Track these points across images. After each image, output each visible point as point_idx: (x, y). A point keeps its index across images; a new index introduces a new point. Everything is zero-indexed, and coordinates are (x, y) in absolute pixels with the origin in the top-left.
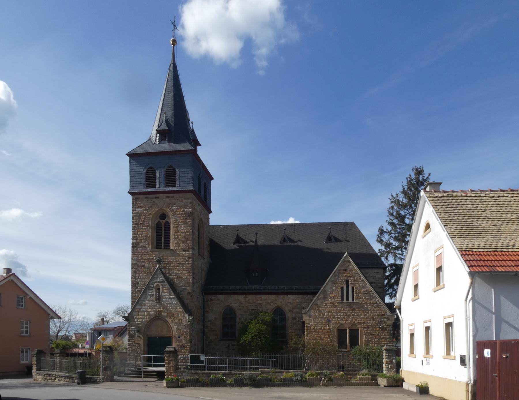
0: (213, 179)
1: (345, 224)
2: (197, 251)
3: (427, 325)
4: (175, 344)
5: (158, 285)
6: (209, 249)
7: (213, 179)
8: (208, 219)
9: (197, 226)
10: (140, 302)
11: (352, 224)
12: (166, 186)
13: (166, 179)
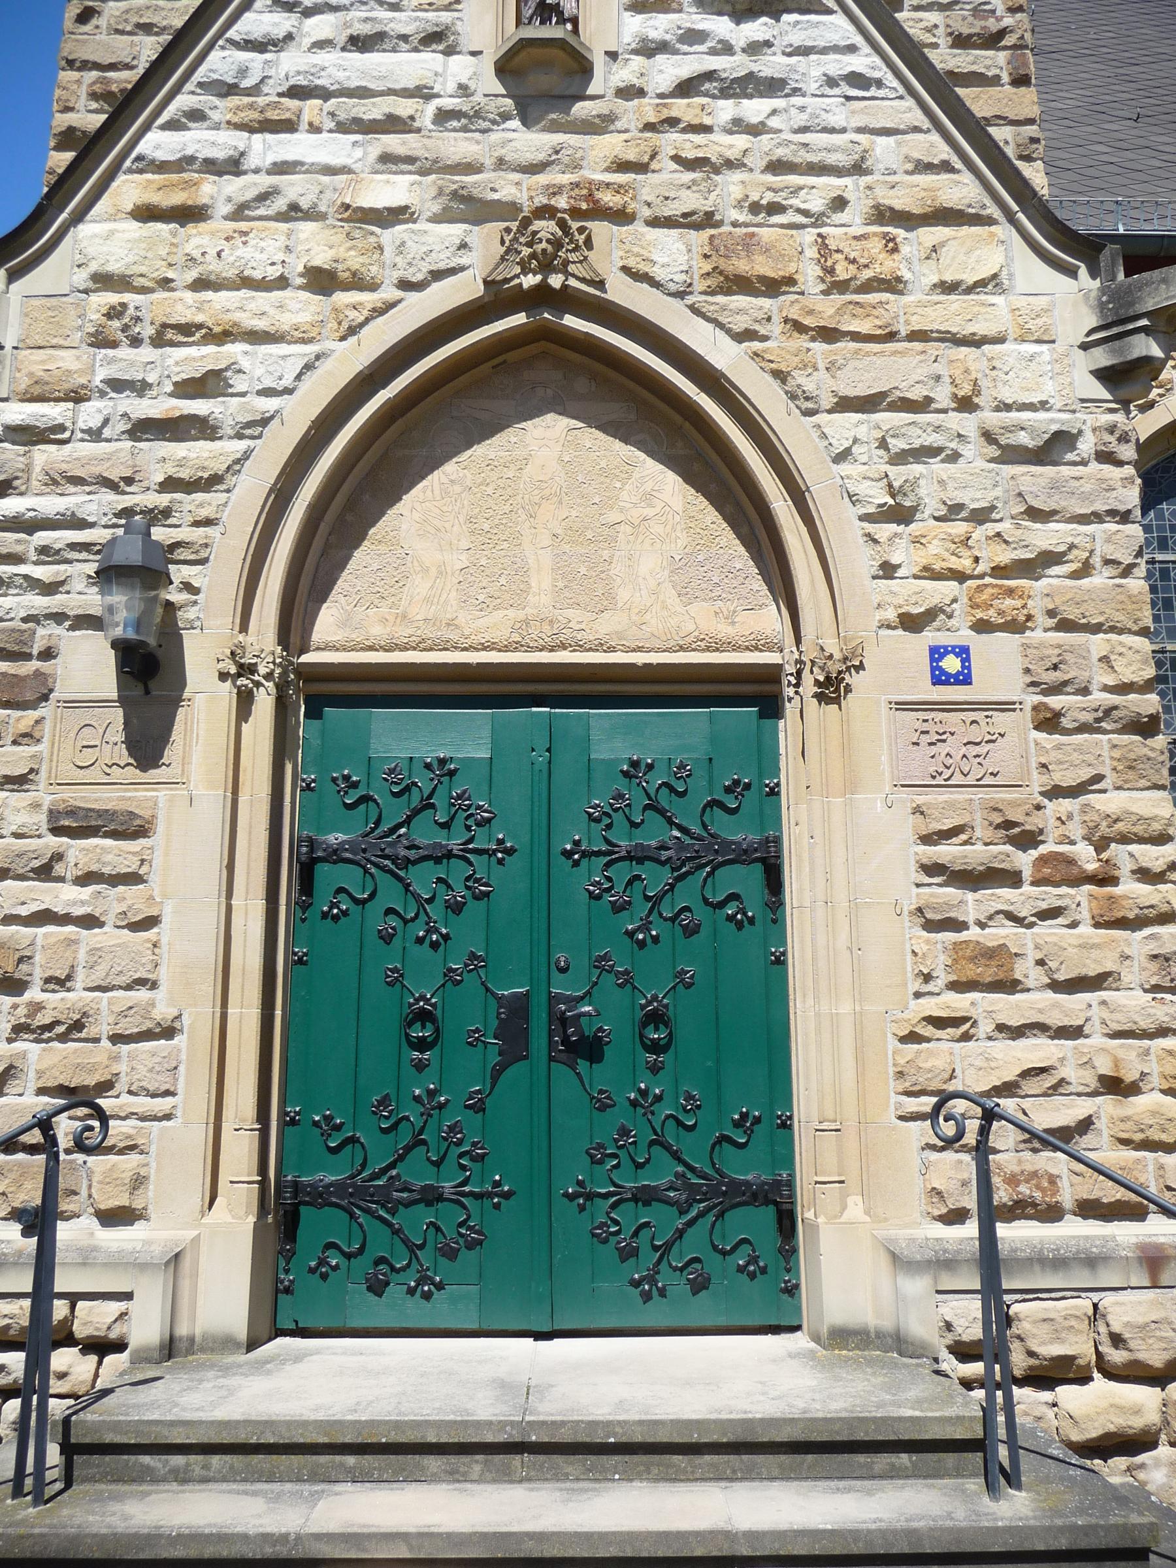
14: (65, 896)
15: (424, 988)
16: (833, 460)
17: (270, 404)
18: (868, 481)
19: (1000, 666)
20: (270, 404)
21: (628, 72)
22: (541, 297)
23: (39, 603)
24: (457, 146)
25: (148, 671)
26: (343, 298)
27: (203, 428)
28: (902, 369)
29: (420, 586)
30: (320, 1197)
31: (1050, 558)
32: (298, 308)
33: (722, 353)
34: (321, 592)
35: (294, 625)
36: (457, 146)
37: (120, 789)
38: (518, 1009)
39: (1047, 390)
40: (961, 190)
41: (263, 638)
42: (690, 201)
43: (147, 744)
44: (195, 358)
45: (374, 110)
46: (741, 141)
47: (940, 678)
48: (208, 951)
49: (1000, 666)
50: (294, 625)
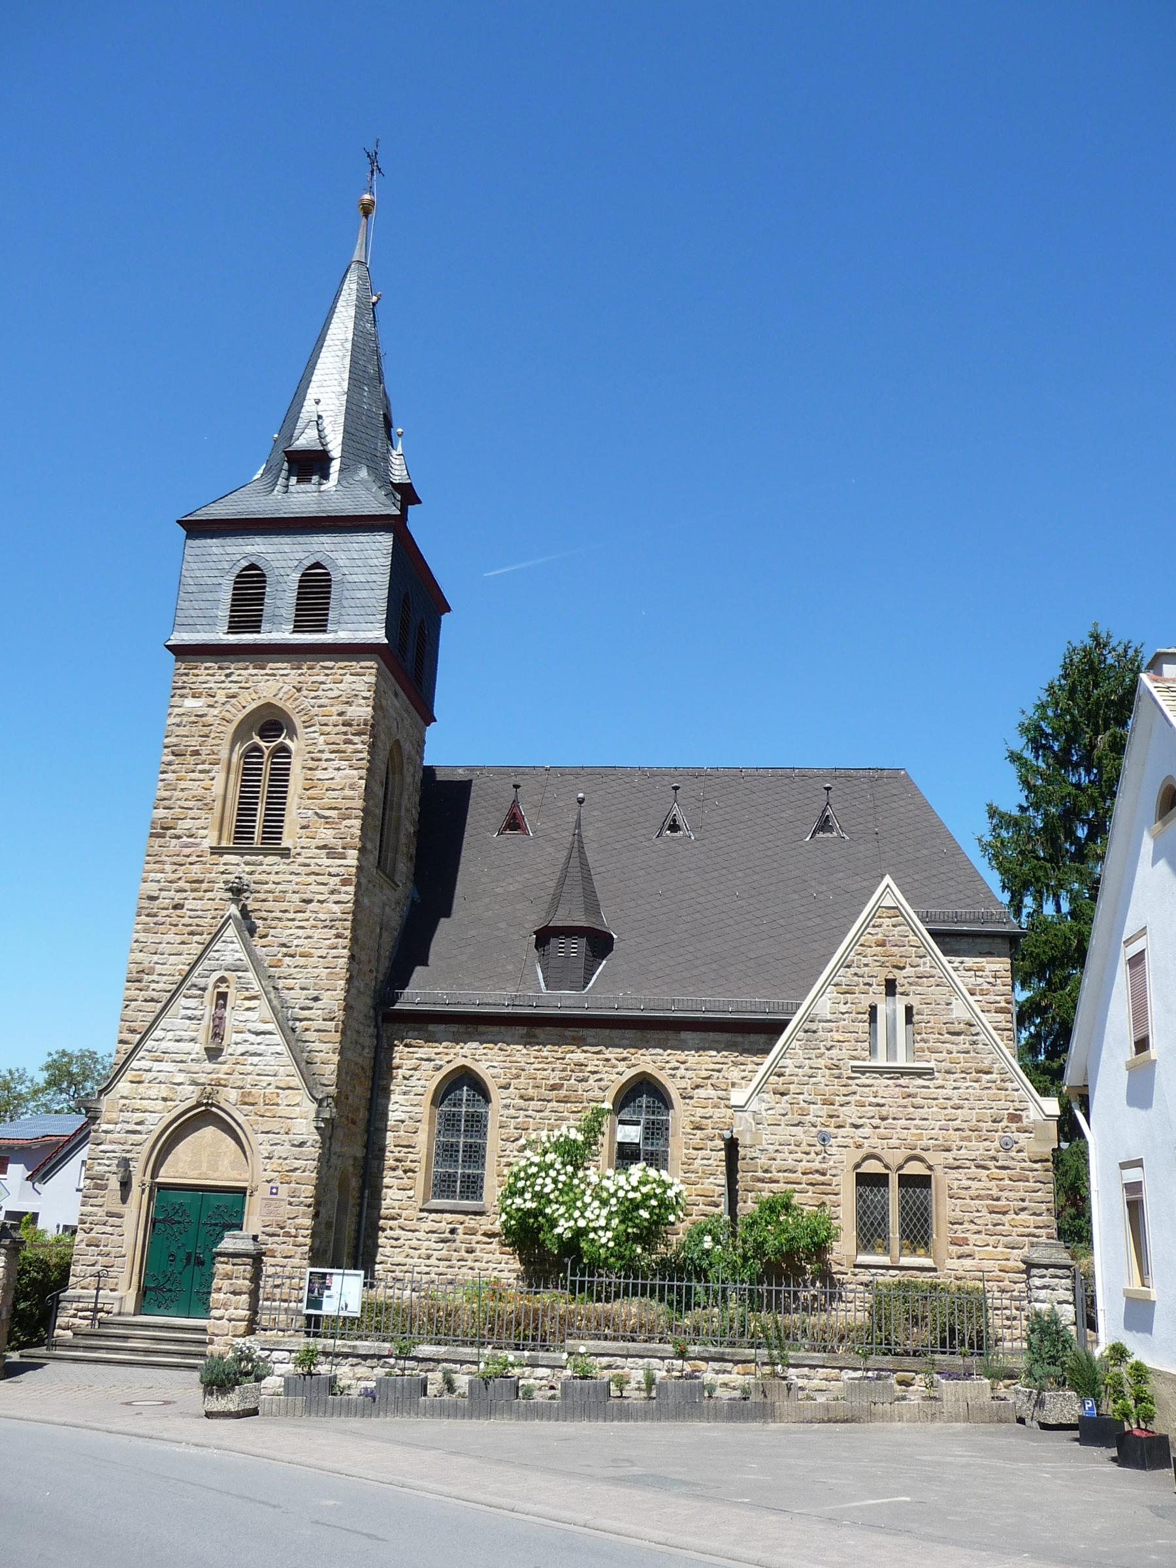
0: (449, 610)
1: (876, 776)
2: (373, 858)
3: (1132, 1175)
4: (254, 1222)
5: (223, 980)
6: (413, 851)
7: (449, 610)
8: (420, 744)
9: (383, 767)
10: (149, 1044)
11: (895, 775)
12: (298, 629)
13: (299, 607)
14: (108, 1229)
15: (173, 1249)
16: (260, 1144)
17: (152, 1127)
18: (265, 1150)
19: (284, 1190)
20: (152, 1127)
21: (230, 1051)
22: (207, 1104)
23: (107, 1169)
24: (195, 1067)
25: (125, 1185)
26: (169, 1103)
27: (139, 1132)
28: (274, 1125)
29: (181, 1164)
30: (151, 1289)
31: (297, 1169)
32: (160, 1105)
33: (241, 1119)
34: (161, 1166)
35: (154, 1174)
36: (195, 1067)
37: (118, 1208)
38: (189, 1254)
39: (304, 1130)
40: (297, 1081)
41: (148, 1178)
42: (239, 1083)
43: (124, 1199)
44: (138, 1116)
45: (178, 1057)
46: (252, 1068)
47: (272, 1193)
48: (133, 1242)
49: (284, 1190)
50: (154, 1174)
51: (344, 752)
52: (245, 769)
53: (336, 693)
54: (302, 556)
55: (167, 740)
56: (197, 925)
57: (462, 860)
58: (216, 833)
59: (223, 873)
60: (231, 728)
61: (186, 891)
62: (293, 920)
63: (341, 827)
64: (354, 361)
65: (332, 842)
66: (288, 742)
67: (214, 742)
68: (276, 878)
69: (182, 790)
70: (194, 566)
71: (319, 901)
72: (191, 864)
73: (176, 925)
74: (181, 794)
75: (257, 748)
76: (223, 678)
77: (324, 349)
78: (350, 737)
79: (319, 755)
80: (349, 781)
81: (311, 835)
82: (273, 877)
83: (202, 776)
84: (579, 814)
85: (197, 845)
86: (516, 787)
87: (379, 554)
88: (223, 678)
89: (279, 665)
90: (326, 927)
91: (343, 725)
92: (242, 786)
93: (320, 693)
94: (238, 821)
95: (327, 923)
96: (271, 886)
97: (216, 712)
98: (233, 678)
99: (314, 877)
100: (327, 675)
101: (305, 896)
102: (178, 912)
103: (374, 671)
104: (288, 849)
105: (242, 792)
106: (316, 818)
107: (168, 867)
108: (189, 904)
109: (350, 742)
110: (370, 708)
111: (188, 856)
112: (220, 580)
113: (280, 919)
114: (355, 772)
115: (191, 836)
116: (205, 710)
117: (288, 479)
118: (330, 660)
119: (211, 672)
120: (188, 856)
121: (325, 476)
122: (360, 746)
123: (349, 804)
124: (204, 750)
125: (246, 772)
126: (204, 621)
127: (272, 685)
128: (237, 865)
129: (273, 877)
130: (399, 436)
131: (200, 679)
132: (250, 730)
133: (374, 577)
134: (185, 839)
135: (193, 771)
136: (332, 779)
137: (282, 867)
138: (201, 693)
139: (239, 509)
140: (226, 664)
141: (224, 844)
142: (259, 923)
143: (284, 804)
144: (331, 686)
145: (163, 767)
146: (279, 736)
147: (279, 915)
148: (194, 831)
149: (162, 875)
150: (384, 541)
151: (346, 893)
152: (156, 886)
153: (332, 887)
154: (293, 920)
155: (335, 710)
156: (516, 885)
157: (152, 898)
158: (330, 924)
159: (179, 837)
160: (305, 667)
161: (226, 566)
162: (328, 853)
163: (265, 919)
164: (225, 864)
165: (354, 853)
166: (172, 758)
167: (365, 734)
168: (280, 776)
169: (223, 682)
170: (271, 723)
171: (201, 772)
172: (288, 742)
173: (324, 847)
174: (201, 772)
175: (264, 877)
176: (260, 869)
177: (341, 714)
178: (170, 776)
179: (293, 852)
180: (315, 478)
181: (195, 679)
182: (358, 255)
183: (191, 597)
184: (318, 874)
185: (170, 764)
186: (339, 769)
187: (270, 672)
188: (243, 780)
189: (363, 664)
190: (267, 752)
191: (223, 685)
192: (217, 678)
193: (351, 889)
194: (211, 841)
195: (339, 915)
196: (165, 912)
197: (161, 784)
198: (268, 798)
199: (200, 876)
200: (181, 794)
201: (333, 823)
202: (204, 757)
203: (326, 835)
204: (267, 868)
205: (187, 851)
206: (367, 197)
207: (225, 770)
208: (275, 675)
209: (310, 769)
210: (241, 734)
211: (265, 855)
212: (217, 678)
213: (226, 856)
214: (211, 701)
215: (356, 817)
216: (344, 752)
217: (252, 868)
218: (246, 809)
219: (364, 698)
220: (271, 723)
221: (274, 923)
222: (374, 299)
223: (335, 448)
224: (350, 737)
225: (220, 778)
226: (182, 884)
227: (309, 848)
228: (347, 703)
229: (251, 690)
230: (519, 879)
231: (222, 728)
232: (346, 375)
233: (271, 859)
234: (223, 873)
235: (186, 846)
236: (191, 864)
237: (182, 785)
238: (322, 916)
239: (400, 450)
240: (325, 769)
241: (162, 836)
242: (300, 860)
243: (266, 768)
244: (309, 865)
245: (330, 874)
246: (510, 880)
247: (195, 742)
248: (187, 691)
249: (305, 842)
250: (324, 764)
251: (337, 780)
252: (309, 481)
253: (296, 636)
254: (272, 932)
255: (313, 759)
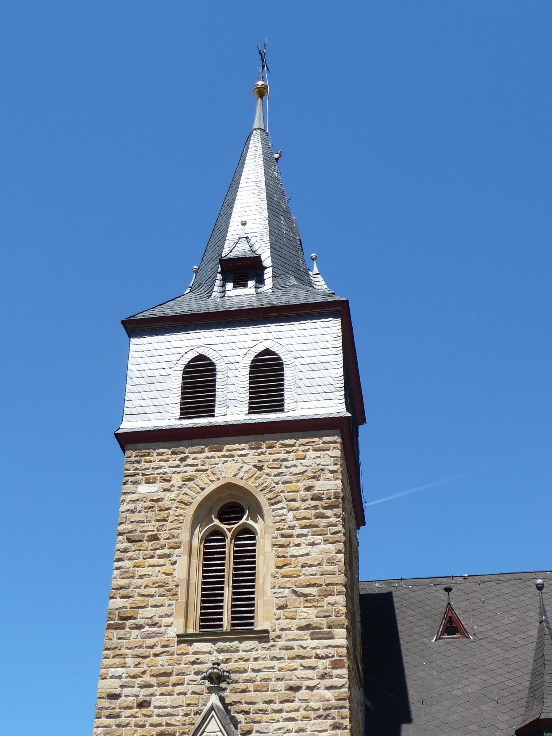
51: (317, 526)
52: (205, 554)
53: (300, 469)
54: (252, 344)
55: (121, 528)
56: (168, 724)
57: (406, 666)
58: (182, 620)
59: (193, 663)
60: (190, 511)
61: (151, 686)
62: (280, 711)
63: (324, 604)
64: (269, 198)
65: (316, 621)
66: (251, 522)
67: (173, 525)
68: (256, 665)
69: (141, 577)
70: (140, 361)
71: (308, 688)
72: (156, 655)
73: (143, 726)
74: (140, 582)
75: (217, 532)
76: (178, 463)
77: (239, 190)
78: (321, 511)
79: (289, 531)
80: (325, 556)
81: (290, 615)
82: (251, 665)
83: (162, 561)
84: (541, 600)
85: (161, 634)
86: (448, 590)
87: (328, 337)
88: (178, 463)
89: (237, 446)
90: (319, 717)
91: (313, 499)
92: (204, 571)
93: (283, 470)
94: (202, 608)
95: (321, 712)
96: (250, 675)
97: (173, 495)
98: (189, 461)
99: (299, 661)
100: (288, 452)
101: (292, 683)
102: (144, 711)
103: (338, 445)
104: (267, 631)
105: (204, 577)
106: (294, 597)
107: (130, 661)
108: (156, 701)
109: (323, 516)
110: (339, 482)
111: (152, 647)
112: (169, 371)
113: (264, 712)
114: (331, 546)
115: (154, 625)
116: (161, 495)
117: (223, 286)
118: (291, 438)
119: (164, 457)
120: (152, 647)
121: (260, 281)
122: (333, 520)
123: (329, 579)
124: (163, 535)
125: (207, 557)
126: (154, 409)
127: (232, 466)
128: (210, 653)
129: (251, 665)
130: (313, 259)
131: (153, 465)
132: (210, 512)
133: (328, 359)
134: (147, 628)
135: (152, 557)
136: (307, 554)
137: (261, 653)
138: (155, 479)
139: (180, 309)
140: (180, 449)
141: (190, 631)
142: (240, 717)
143: (253, 587)
144: (295, 462)
145: (118, 555)
146: (241, 518)
147: (265, 706)
148: (157, 619)
149: (123, 670)
150: (334, 325)
151: (339, 676)
152: (117, 683)
153: (321, 671)
154: (280, 711)
155: (301, 485)
156: (474, 686)
157: (113, 697)
158: (325, 713)
159: (139, 627)
160: (264, 446)
161: (173, 358)
162: (311, 634)
163: (247, 713)
164: (195, 653)
165: (342, 632)
166: (127, 544)
167: (337, 507)
168: (246, 560)
169: (178, 466)
170: (231, 505)
171: (160, 557)
172: (251, 522)
173: (308, 627)
174: (160, 557)
175: (241, 665)
176: (236, 656)
177: (308, 489)
178: (126, 564)
179: (272, 635)
180: (251, 283)
181: (147, 465)
182: (258, 123)
183: (140, 388)
184: (303, 658)
185: (125, 551)
186: (313, 544)
187: (227, 453)
188: (204, 565)
189: (325, 439)
190: (229, 535)
191: (178, 470)
192: (171, 463)
193: (344, 672)
194: (177, 628)
195: (334, 702)
196: (128, 712)
197: (116, 572)
198: (234, 581)
199: (169, 669)
200: (140, 582)
201: (314, 601)
202: (162, 542)
203: (308, 614)
204: (245, 655)
205: (150, 642)
206: (260, 83)
207: (187, 553)
208: (232, 456)
209: (282, 546)
210: (200, 518)
211: (241, 640)
212: (171, 463)
213: (195, 644)
214: (166, 485)
215: (340, 593)
216: (317, 526)
217: (227, 655)
218: (211, 595)
219: (332, 472)
220: (231, 505)
221: (257, 717)
222: (276, 156)
223: (267, 261)
224: (321, 511)
225: (182, 562)
226: (147, 678)
227: (290, 629)
228: (313, 477)
229: (209, 472)
230: (474, 680)
231: (179, 512)
232: (265, 206)
233: (247, 645)
234: (193, 663)
235: (149, 636)
236: (156, 655)
237: (141, 571)
238: (313, 704)
239: (316, 270)
240: (298, 545)
241: (122, 627)
242: (281, 643)
243: (229, 550)
244: (292, 648)
245: (317, 657)
246: (466, 682)
247: (152, 527)
248: (140, 477)
249: (284, 623)
250: (297, 540)
251: (313, 555)
252: (245, 285)
253: (253, 416)
254: (256, 727)
255: (283, 536)
